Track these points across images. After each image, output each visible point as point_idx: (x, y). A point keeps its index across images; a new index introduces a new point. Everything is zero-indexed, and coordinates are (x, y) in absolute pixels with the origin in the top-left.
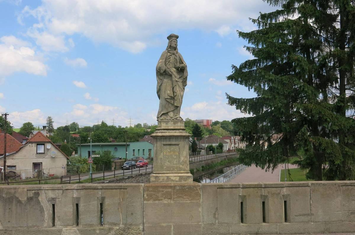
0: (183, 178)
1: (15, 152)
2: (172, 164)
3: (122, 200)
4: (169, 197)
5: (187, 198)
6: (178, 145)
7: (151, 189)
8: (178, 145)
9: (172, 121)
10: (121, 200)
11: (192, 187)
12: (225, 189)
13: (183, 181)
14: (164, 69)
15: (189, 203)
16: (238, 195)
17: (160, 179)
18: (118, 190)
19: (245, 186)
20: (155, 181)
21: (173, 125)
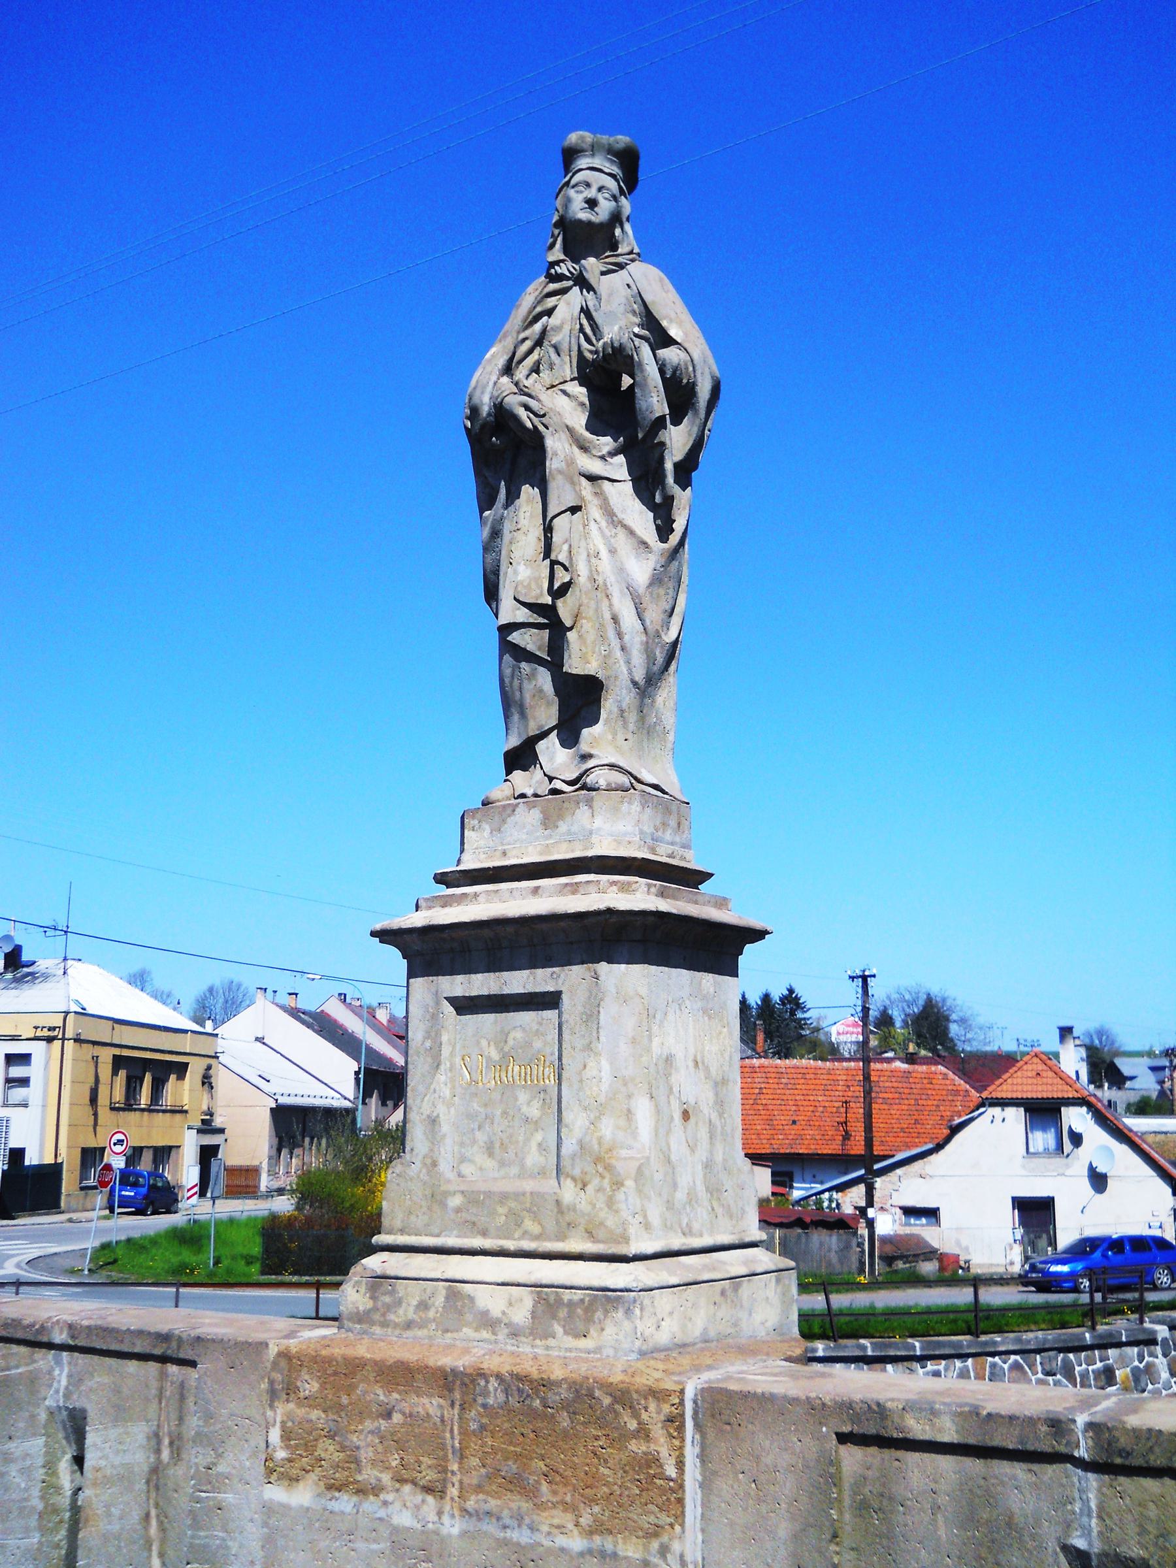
0: (559, 1301)
1: (930, 1146)
2: (514, 1170)
3: (172, 1457)
4: (430, 1476)
5: (566, 1507)
6: (549, 1001)
7: (310, 1386)
8: (549, 1001)
9: (531, 806)
10: (165, 1455)
11: (607, 1401)
12: (913, 1458)
13: (558, 1329)
14: (486, 399)
15: (582, 1554)
16: (1052, 1546)
17: (399, 1302)
18: (153, 1366)
19: (1123, 1442)
20: (368, 1312)
21: (540, 832)
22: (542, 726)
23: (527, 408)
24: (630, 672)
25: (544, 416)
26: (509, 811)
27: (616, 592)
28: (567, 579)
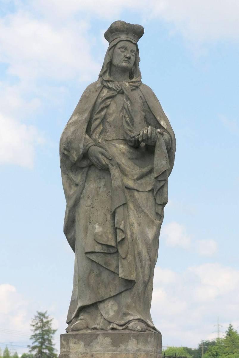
9: (106, 335)
22: (103, 297)
23: (103, 154)
24: (143, 277)
25: (111, 160)
26: (94, 337)
27: (140, 242)
28: (123, 237)
